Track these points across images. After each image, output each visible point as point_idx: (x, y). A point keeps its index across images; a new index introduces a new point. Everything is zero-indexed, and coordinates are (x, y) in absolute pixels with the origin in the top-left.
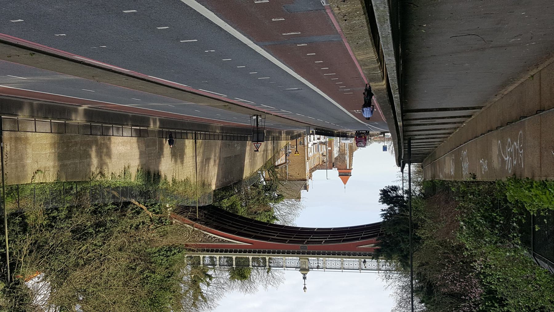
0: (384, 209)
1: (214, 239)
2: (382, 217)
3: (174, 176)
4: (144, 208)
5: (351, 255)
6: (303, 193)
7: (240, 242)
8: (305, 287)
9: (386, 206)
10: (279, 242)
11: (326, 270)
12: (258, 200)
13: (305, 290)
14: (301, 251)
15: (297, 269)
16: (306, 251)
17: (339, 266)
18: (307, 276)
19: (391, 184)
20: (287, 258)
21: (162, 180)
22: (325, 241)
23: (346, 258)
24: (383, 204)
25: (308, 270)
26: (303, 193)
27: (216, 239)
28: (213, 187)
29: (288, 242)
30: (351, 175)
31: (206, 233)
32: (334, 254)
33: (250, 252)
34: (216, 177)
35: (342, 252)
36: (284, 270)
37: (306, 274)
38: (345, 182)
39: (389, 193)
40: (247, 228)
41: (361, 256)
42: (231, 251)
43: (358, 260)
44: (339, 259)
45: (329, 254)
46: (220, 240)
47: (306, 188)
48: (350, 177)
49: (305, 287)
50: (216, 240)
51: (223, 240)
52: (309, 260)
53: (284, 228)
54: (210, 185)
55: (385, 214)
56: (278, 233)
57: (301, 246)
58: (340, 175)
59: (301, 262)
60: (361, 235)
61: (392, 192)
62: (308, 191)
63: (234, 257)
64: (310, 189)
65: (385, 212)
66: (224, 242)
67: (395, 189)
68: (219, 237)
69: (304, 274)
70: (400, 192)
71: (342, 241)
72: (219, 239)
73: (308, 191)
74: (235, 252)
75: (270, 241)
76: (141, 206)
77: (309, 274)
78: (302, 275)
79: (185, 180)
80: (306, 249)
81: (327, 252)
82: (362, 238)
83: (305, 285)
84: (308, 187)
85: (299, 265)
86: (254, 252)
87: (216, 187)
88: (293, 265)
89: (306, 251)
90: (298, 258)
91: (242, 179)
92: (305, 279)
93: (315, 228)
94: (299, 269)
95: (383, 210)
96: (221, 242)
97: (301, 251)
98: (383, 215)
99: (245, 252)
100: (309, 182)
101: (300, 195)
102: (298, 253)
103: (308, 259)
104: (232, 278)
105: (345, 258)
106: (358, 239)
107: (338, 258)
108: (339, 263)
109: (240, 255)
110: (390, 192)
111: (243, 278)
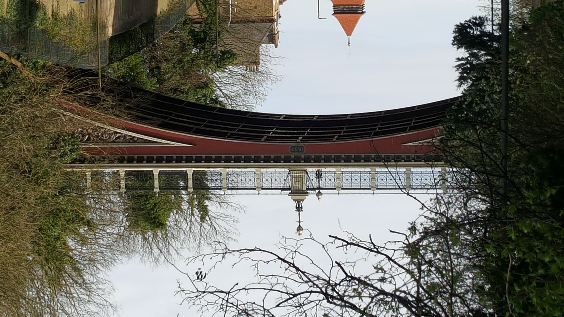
0: (460, 58)
1: (113, 137)
2: (458, 69)
3: (55, 5)
4: (19, 64)
5: (390, 161)
6: (266, 48)
7: (169, 142)
8: (300, 226)
9: (463, 53)
10: (248, 139)
11: (342, 191)
12: (180, 61)
13: (301, 232)
14: (293, 156)
15: (284, 192)
16: (303, 156)
17: (367, 184)
18: (304, 204)
19: (478, 14)
20: (263, 170)
21: (40, 14)
22: (339, 136)
23: (380, 166)
24: (458, 48)
25: (305, 193)
26: (266, 48)
27: (119, 136)
28: (110, 32)
29: (265, 140)
30: (363, 13)
31: (97, 124)
32: (357, 159)
33: (189, 160)
34: (113, 10)
35: (373, 155)
36: (373, 194)
37: (303, 200)
38: (349, 29)
39: (469, 30)
40: (173, 114)
41: (410, 161)
42: (150, 160)
43: (404, 170)
44: (368, 170)
45: (348, 160)
46: (128, 138)
47: (272, 39)
48: (362, 17)
49: (300, 226)
50: (119, 137)
51: (134, 137)
52: (307, 173)
53: (250, 115)
54: (104, 27)
55: (462, 64)
56: (240, 125)
57: (292, 147)
58: (336, 13)
59: (292, 177)
60: (410, 124)
61: (474, 27)
62: (276, 47)
63: (156, 172)
64: (281, 38)
65: (463, 62)
66: (135, 141)
67: (479, 22)
68: (125, 132)
69: (299, 201)
70: (488, 28)
71: (373, 135)
72: (125, 136)
73: (276, 47)
74: (159, 160)
75: (229, 138)
76: (13, 61)
77: (310, 200)
78: (294, 204)
79: (68, 15)
80: (302, 152)
81: (343, 156)
82: (412, 129)
83: (299, 222)
84: (276, 36)
85: (288, 184)
86: (198, 160)
87: (114, 31)
88: (275, 184)
89: (303, 156)
90: (287, 170)
91: (155, 15)
92: (299, 211)
93: (314, 116)
94: (289, 192)
95: (459, 59)
96: (129, 142)
97: (293, 156)
98: (459, 66)
99: (179, 160)
100: (281, 27)
101: (257, 55)
102: (287, 160)
103: (306, 171)
104: (134, 225)
105: (380, 167)
106: (404, 130)
107: (365, 166)
108: (368, 177)
109: (168, 167)
110: (472, 28)
111: (158, 227)
